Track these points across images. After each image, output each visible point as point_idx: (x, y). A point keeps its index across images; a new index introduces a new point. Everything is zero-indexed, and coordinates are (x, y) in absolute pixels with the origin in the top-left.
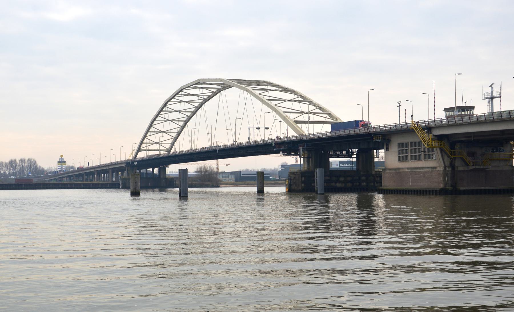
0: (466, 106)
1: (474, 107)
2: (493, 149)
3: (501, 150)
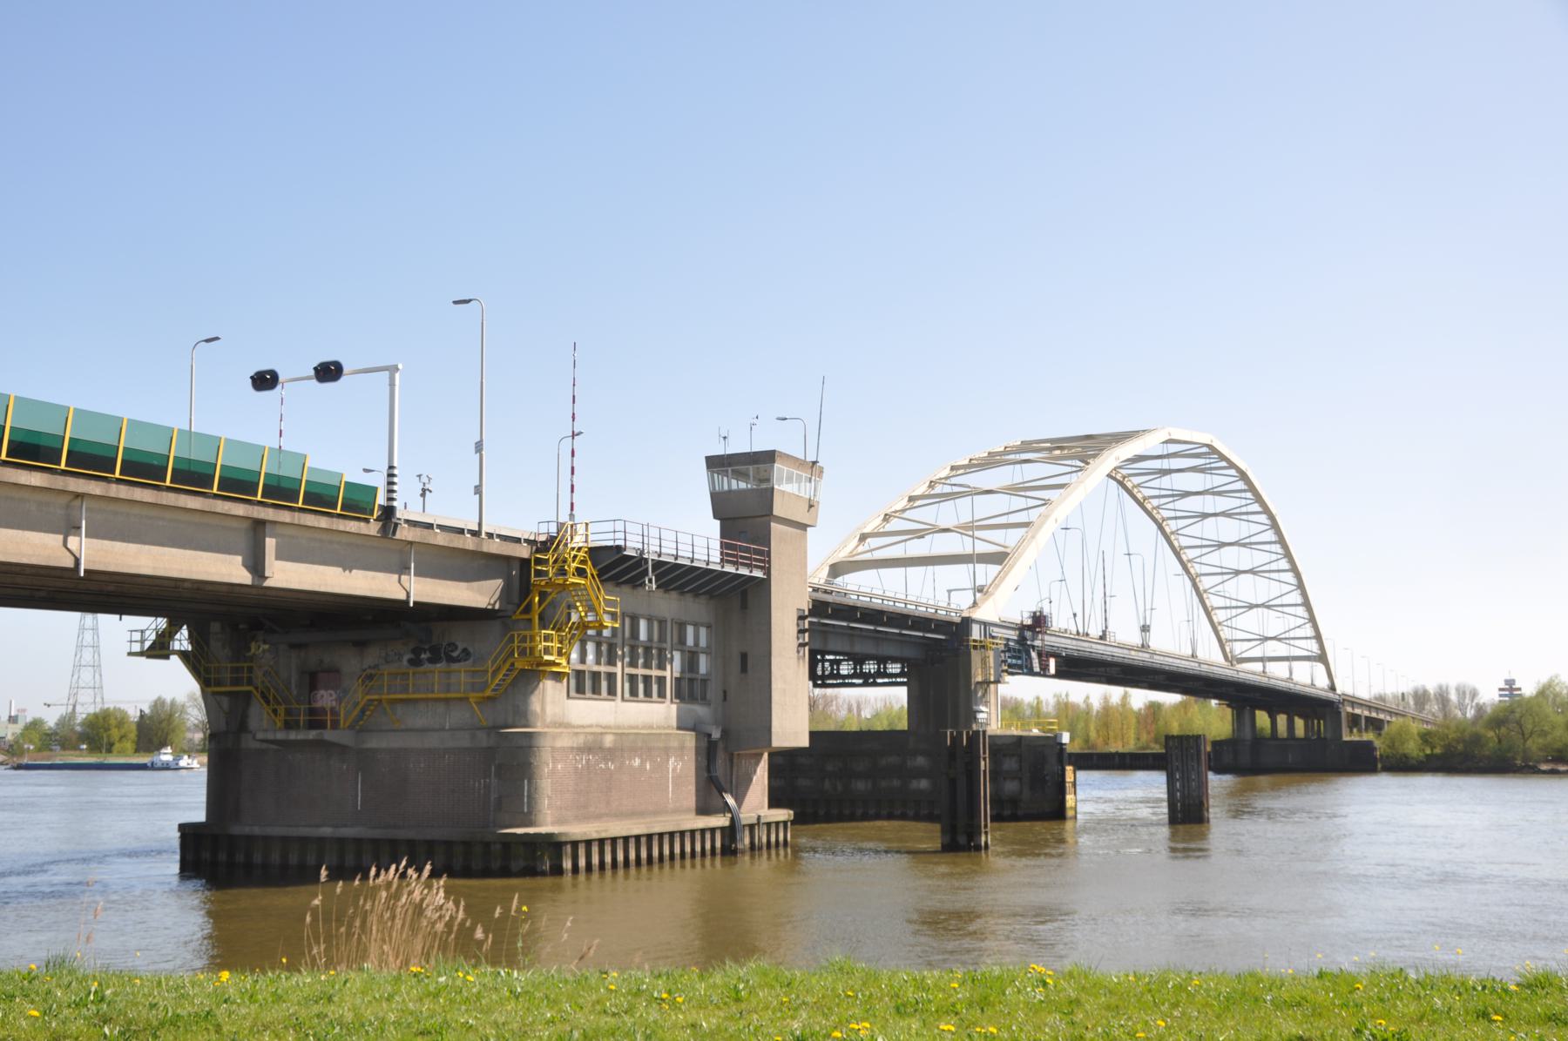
0: (728, 455)
1: (377, 488)
2: (417, 651)
3: (455, 654)
